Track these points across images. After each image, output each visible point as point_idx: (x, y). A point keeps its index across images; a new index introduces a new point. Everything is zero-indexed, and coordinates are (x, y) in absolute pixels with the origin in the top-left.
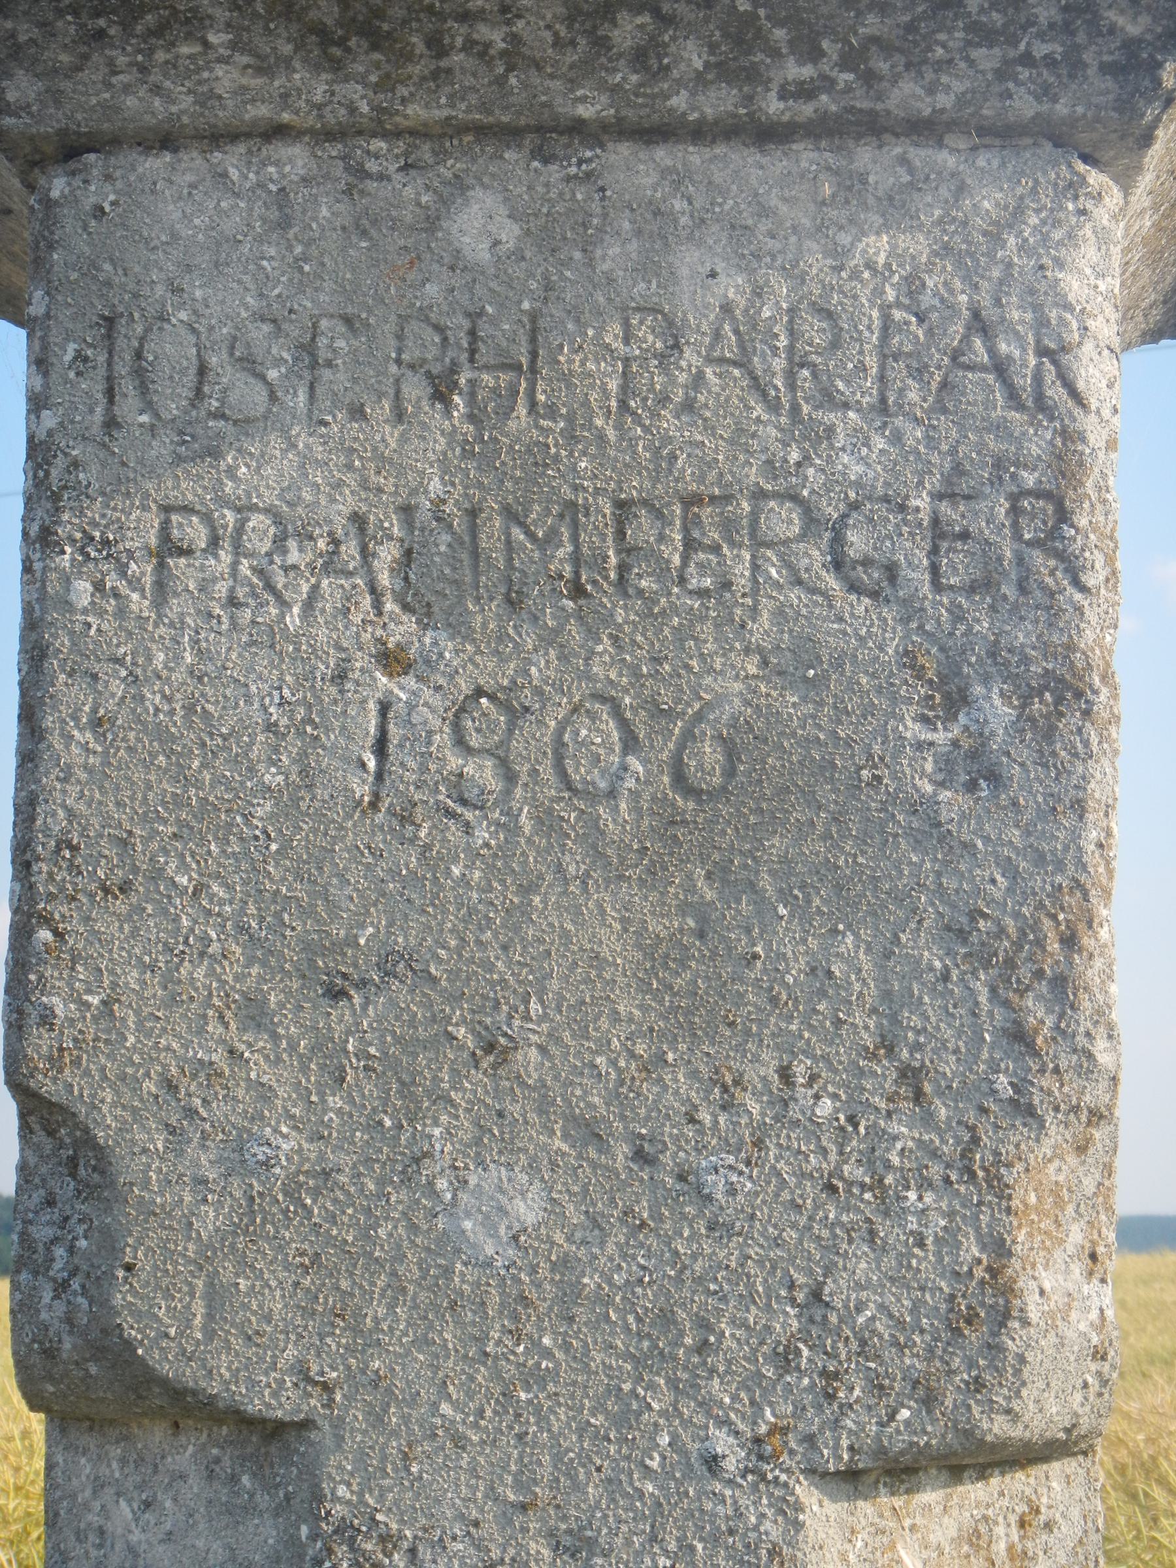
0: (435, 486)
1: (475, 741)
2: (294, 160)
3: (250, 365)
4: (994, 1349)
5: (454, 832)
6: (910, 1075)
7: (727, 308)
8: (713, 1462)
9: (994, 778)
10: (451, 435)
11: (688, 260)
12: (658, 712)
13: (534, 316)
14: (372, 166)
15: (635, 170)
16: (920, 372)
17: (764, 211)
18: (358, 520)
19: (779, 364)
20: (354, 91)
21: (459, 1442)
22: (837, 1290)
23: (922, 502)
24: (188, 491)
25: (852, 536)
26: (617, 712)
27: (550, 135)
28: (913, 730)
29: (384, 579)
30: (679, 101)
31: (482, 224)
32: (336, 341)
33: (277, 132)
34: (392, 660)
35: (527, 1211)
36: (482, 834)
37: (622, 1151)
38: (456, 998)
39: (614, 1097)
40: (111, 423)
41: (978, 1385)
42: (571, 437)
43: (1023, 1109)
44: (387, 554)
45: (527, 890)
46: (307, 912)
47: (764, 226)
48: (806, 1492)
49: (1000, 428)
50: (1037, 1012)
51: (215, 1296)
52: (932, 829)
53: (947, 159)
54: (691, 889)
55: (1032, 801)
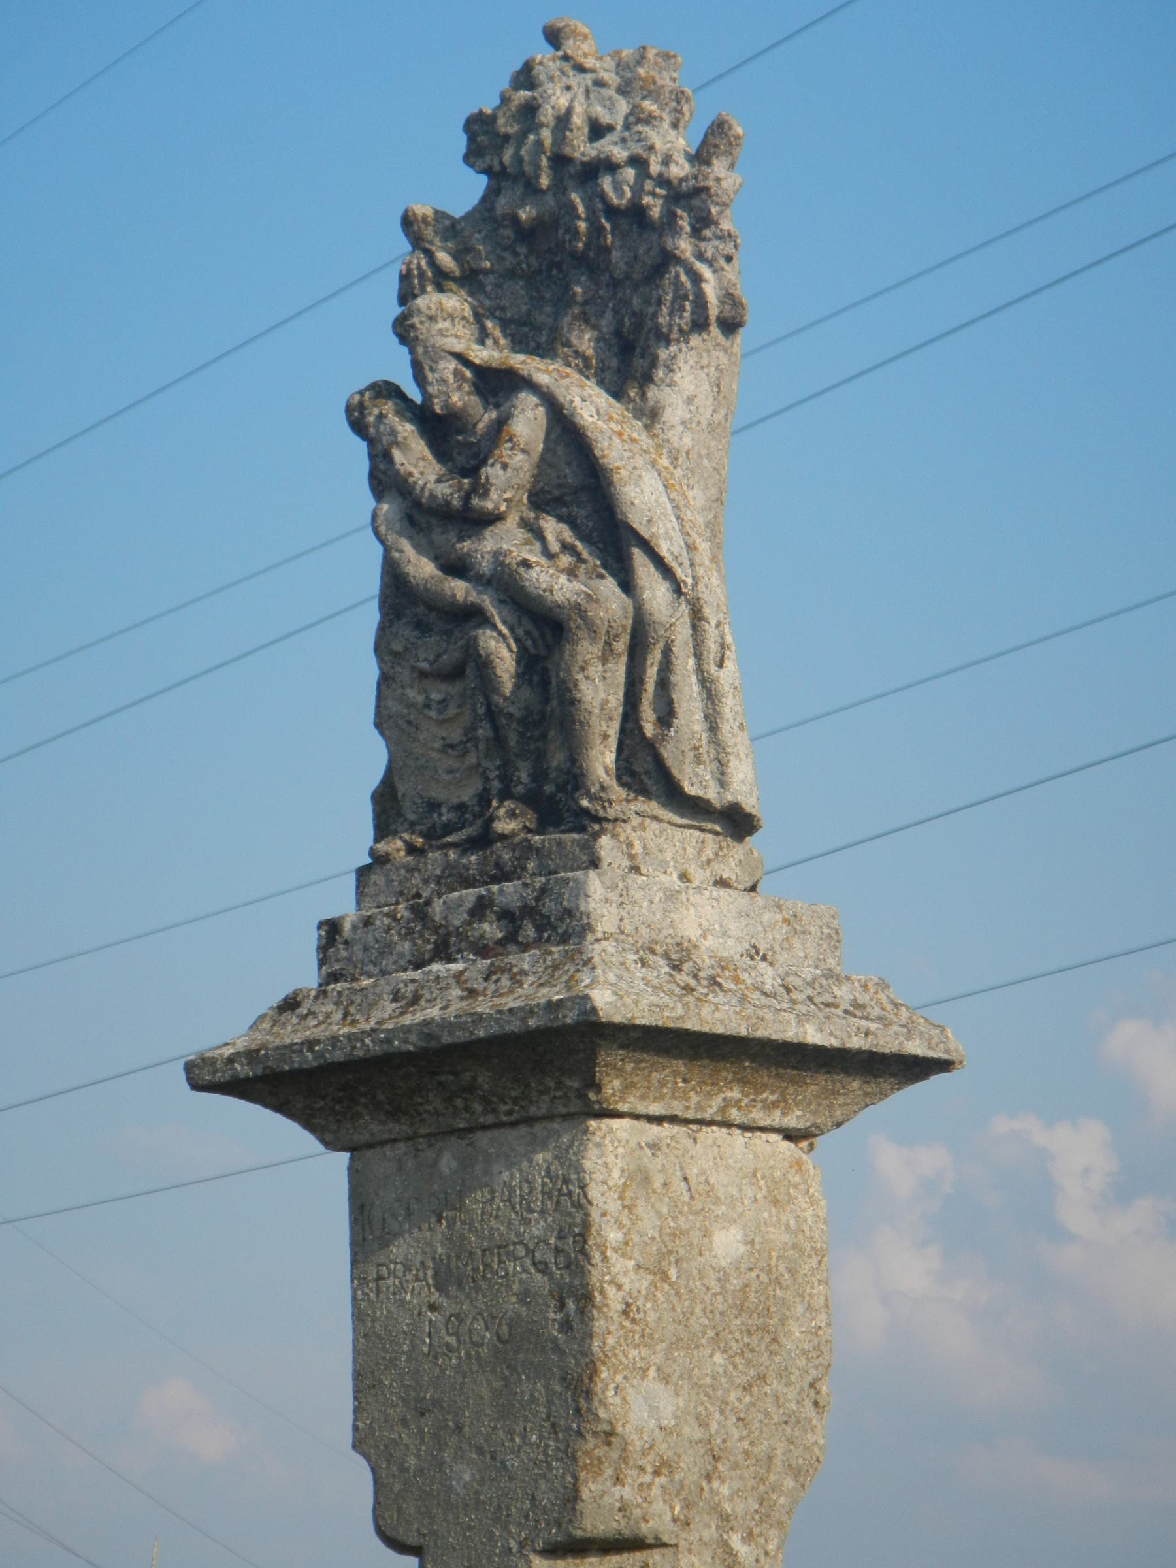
0: (440, 1250)
1: (451, 1331)
2: (402, 1147)
3: (395, 1216)
4: (574, 1509)
5: (447, 1362)
6: (554, 1425)
7: (505, 1183)
8: (510, 1549)
9: (571, 1328)
10: (442, 1233)
11: (496, 1168)
12: (494, 1318)
13: (460, 1191)
14: (420, 1147)
15: (483, 1139)
16: (550, 1198)
17: (513, 1150)
18: (422, 1263)
19: (518, 1200)
20: (405, 1128)
21: (454, 1549)
22: (539, 1496)
23: (552, 1241)
24: (382, 1259)
25: (537, 1254)
26: (483, 1319)
27: (461, 1133)
28: (552, 1315)
29: (430, 1281)
30: (481, 1120)
31: (447, 1164)
32: (415, 1207)
33: (395, 1140)
34: (433, 1307)
35: (467, 1477)
36: (454, 1361)
37: (488, 1456)
38: (449, 1413)
39: (486, 1440)
40: (364, 1239)
41: (570, 1521)
42: (470, 1229)
43: (579, 1434)
44: (430, 1273)
45: (464, 1377)
46: (415, 1390)
47: (513, 1154)
48: (532, 1556)
49: (570, 1214)
50: (583, 1403)
51: (400, 1509)
52: (557, 1349)
53: (556, 1126)
54: (502, 1372)
55: (579, 1336)
